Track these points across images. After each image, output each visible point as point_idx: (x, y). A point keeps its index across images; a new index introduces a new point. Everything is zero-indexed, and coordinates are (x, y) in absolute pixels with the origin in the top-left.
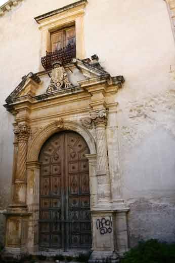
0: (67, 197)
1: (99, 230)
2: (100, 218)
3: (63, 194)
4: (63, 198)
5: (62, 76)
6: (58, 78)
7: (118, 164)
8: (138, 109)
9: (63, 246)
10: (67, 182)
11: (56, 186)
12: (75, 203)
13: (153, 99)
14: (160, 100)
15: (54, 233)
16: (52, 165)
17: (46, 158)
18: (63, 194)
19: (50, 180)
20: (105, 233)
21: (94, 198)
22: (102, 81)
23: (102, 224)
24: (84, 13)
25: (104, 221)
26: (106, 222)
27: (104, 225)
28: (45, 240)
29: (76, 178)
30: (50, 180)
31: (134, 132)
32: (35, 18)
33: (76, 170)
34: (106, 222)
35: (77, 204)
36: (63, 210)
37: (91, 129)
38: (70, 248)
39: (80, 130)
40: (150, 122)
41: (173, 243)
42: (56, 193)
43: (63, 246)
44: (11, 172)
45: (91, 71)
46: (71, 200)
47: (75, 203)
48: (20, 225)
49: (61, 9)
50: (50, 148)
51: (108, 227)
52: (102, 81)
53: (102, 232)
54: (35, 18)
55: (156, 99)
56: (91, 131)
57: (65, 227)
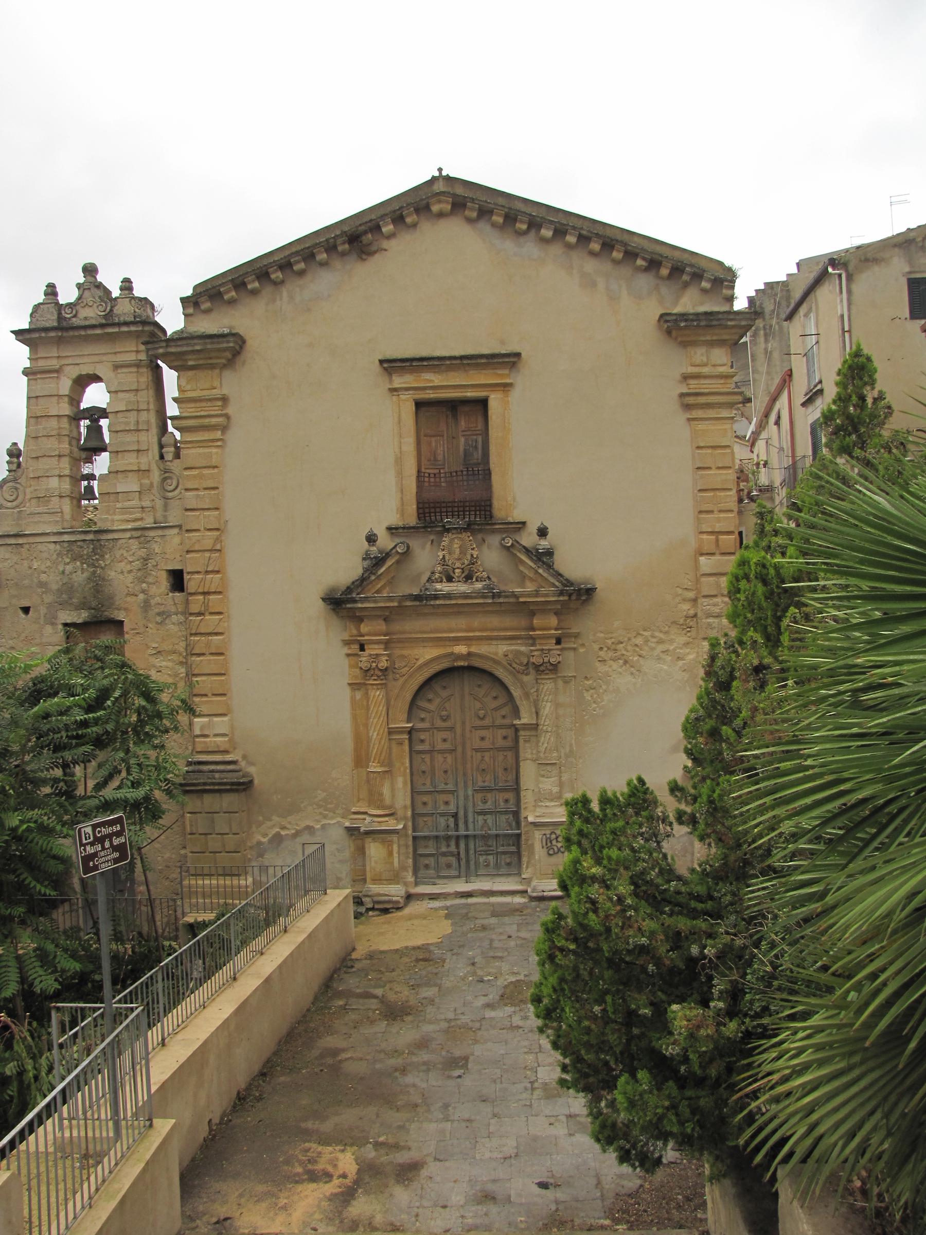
0: (470, 793)
1: (545, 849)
2: (548, 832)
3: (461, 785)
4: (461, 794)
5: (469, 557)
6: (459, 559)
7: (573, 741)
8: (613, 646)
9: (463, 873)
10: (469, 766)
11: (446, 772)
12: (486, 802)
13: (642, 632)
14: (653, 637)
15: (444, 854)
16: (435, 731)
17: (423, 715)
18: (461, 785)
19: (432, 760)
20: (555, 853)
21: (527, 798)
22: (561, 598)
23: (551, 842)
24: (510, 385)
25: (553, 836)
26: (557, 838)
27: (554, 842)
28: (427, 867)
29: (487, 759)
30: (432, 760)
31: (604, 687)
32: (381, 362)
33: (486, 744)
34: (557, 838)
35: (489, 803)
36: (461, 813)
37: (527, 674)
38: (477, 876)
39: (500, 673)
40: (632, 674)
41: (367, 1193)
42: (446, 784)
43: (463, 873)
44: (349, 744)
45: (540, 571)
46: (479, 796)
47: (485, 801)
48: (395, 847)
49: (455, 358)
50: (430, 696)
51: (559, 845)
52: (561, 598)
53: (551, 852)
54: (381, 362)
55: (646, 633)
56: (525, 679)
57: (467, 845)
